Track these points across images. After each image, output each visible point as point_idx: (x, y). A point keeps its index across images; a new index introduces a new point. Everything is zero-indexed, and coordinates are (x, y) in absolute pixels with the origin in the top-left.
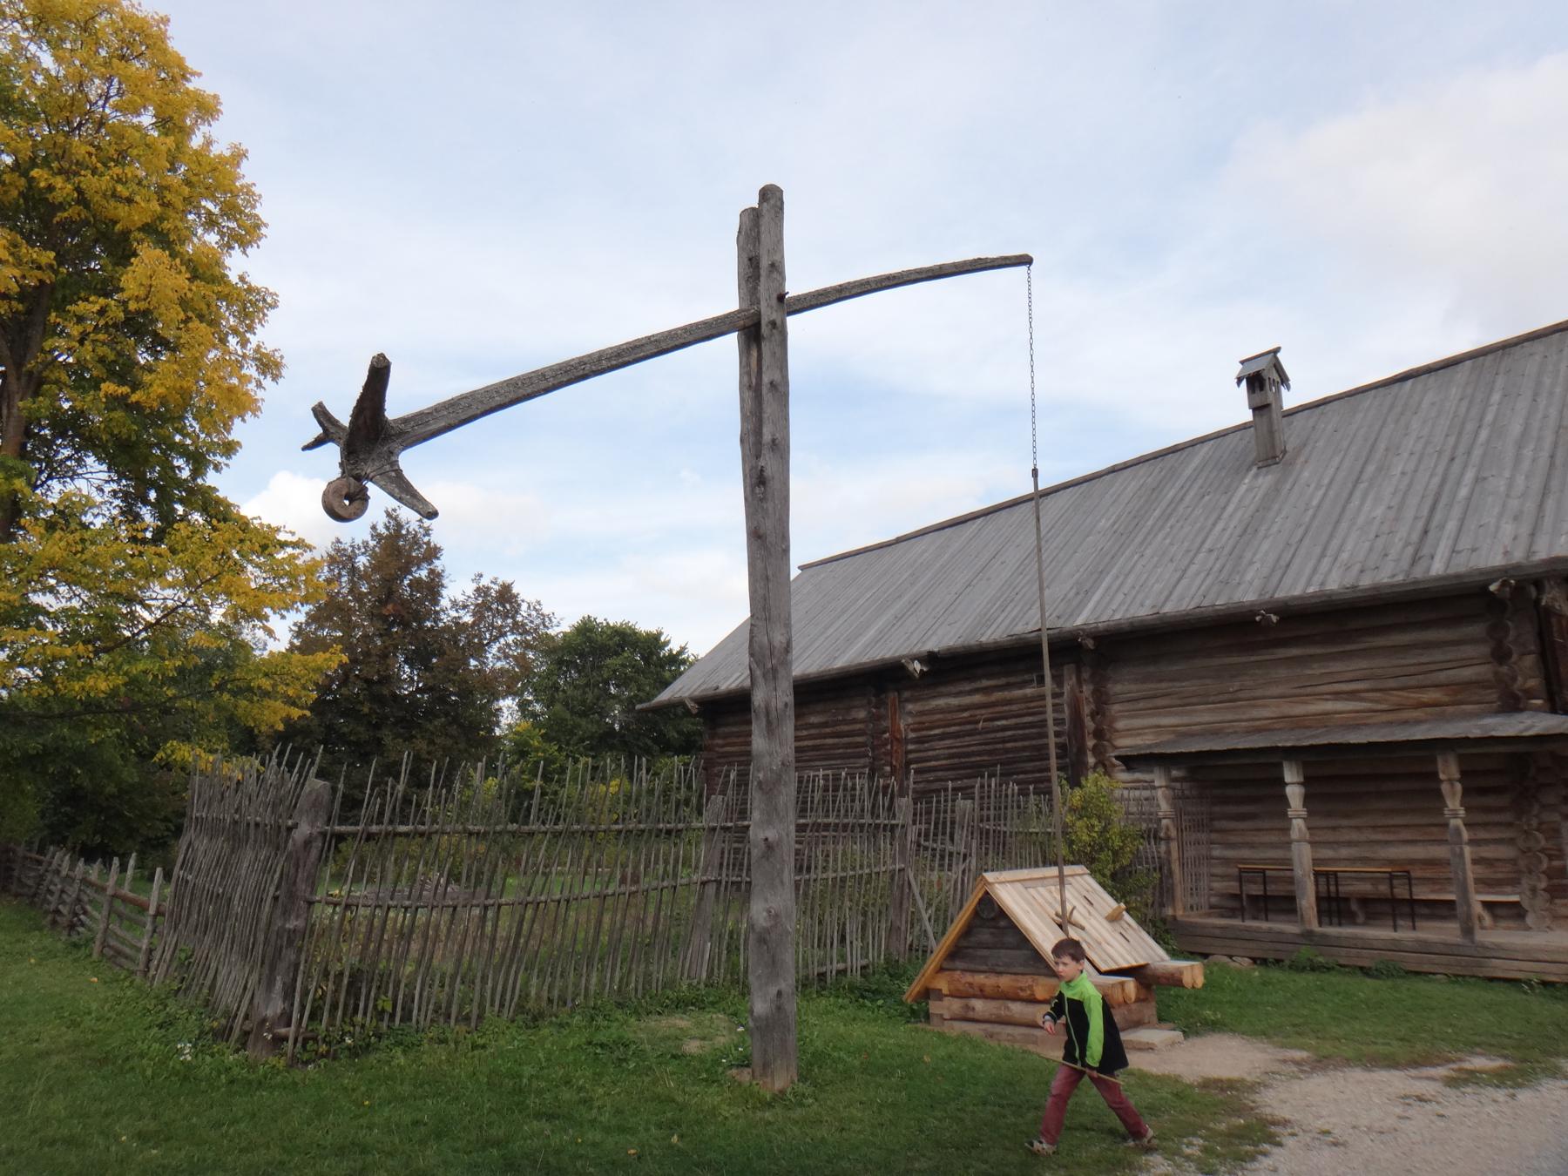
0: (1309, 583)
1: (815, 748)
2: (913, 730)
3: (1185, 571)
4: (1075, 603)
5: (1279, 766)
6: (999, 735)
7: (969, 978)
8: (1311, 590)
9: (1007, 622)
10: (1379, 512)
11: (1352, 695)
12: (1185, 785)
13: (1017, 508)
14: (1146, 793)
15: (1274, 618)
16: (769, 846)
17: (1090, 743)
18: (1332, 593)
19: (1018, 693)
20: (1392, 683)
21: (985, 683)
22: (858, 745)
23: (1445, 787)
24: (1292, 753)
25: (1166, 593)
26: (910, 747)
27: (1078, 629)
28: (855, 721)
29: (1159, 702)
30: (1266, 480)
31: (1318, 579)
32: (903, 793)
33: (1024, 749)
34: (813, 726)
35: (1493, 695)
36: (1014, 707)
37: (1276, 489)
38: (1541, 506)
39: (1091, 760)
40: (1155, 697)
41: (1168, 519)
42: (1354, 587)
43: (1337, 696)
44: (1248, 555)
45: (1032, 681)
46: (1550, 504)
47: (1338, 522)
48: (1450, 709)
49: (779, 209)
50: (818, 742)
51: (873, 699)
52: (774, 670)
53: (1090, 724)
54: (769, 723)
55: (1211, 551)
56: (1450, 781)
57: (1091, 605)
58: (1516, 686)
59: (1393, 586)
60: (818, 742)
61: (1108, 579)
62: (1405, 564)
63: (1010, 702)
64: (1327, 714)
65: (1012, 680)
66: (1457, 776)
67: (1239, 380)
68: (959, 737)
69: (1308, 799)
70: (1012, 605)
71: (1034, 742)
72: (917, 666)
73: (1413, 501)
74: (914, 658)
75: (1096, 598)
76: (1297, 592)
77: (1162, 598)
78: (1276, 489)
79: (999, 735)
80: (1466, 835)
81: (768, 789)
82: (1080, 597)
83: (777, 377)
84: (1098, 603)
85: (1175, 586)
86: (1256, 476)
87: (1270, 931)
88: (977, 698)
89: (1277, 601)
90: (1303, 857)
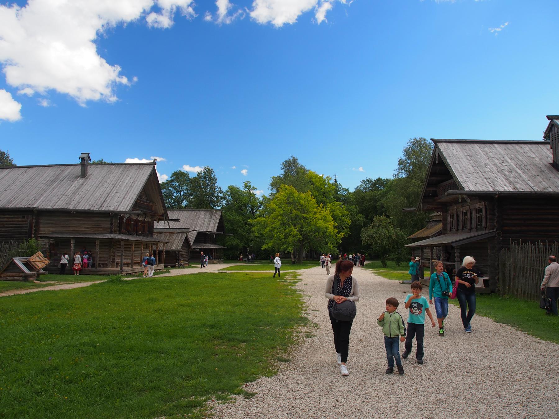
0: (82, 207)
3: (60, 199)
4: (34, 201)
6: (10, 228)
7: (7, 274)
8: (82, 209)
9: (16, 203)
10: (99, 195)
11: (88, 228)
13: (20, 169)
14: (44, 243)
15: (75, 213)
17: (33, 232)
18: (86, 210)
20: (94, 227)
23: (97, 245)
25: (55, 203)
27: (34, 208)
29: (50, 225)
30: (81, 181)
31: (84, 207)
35: (110, 230)
37: (84, 182)
38: (122, 200)
39: (33, 236)
40: (49, 224)
41: (59, 185)
42: (90, 209)
43: (85, 227)
44: (73, 198)
46: (124, 200)
47: (91, 195)
53: (34, 228)
55: (66, 195)
56: (98, 244)
57: (37, 203)
59: (95, 211)
61: (43, 197)
62: (99, 207)
63: (14, 221)
64: (82, 230)
65: (15, 216)
67: (80, 158)
69: (75, 246)
70: (17, 199)
73: (105, 194)
75: (39, 201)
76: (80, 209)
77: (54, 204)
78: (84, 182)
79: (10, 228)
82: (35, 200)
84: (40, 202)
85: (57, 203)
86: (80, 179)
89: (76, 210)
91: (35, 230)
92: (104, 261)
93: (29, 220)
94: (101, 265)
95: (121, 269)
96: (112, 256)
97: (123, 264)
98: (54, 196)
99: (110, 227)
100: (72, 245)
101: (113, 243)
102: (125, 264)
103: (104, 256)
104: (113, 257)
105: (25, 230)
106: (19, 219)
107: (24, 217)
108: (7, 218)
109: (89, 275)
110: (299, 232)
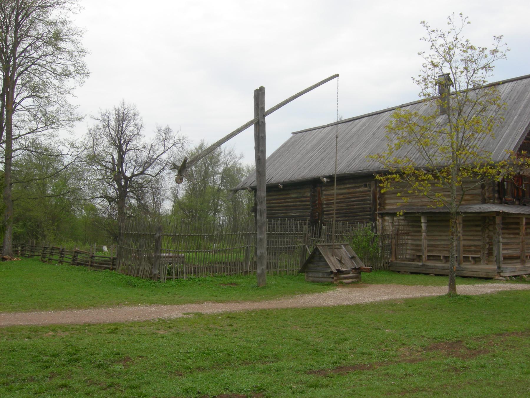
1: (294, 206)
2: (325, 201)
5: (420, 217)
12: (403, 221)
16: (261, 240)
19: (358, 190)
21: (348, 186)
22: (307, 205)
24: (423, 213)
26: (324, 206)
28: (306, 197)
32: (305, 224)
33: (359, 208)
34: (293, 198)
35: (480, 198)
36: (357, 194)
45: (362, 186)
48: (471, 201)
49: (263, 93)
50: (294, 203)
51: (312, 189)
52: (262, 202)
53: (378, 201)
54: (261, 213)
58: (486, 196)
60: (294, 203)
63: (355, 193)
65: (357, 185)
66: (461, 222)
68: (339, 203)
69: (427, 227)
71: (362, 206)
72: (325, 179)
74: (324, 177)
79: (352, 203)
80: (462, 238)
81: (261, 228)
83: (263, 135)
87: (415, 265)
88: (346, 191)
90: (424, 243)
91: (380, 204)
92: (476, 252)
93: (372, 189)
94: (470, 259)
95: (499, 268)
96: (488, 243)
97: (502, 259)
98: (427, 154)
99: (482, 192)
100: (423, 225)
101: (487, 221)
102: (505, 258)
103: (476, 243)
104: (490, 245)
105: (369, 204)
106: (361, 189)
107: (366, 186)
108: (348, 188)
109: (428, 274)
110: (62, 38)
